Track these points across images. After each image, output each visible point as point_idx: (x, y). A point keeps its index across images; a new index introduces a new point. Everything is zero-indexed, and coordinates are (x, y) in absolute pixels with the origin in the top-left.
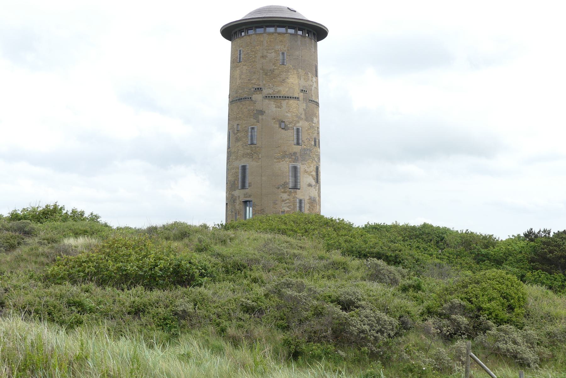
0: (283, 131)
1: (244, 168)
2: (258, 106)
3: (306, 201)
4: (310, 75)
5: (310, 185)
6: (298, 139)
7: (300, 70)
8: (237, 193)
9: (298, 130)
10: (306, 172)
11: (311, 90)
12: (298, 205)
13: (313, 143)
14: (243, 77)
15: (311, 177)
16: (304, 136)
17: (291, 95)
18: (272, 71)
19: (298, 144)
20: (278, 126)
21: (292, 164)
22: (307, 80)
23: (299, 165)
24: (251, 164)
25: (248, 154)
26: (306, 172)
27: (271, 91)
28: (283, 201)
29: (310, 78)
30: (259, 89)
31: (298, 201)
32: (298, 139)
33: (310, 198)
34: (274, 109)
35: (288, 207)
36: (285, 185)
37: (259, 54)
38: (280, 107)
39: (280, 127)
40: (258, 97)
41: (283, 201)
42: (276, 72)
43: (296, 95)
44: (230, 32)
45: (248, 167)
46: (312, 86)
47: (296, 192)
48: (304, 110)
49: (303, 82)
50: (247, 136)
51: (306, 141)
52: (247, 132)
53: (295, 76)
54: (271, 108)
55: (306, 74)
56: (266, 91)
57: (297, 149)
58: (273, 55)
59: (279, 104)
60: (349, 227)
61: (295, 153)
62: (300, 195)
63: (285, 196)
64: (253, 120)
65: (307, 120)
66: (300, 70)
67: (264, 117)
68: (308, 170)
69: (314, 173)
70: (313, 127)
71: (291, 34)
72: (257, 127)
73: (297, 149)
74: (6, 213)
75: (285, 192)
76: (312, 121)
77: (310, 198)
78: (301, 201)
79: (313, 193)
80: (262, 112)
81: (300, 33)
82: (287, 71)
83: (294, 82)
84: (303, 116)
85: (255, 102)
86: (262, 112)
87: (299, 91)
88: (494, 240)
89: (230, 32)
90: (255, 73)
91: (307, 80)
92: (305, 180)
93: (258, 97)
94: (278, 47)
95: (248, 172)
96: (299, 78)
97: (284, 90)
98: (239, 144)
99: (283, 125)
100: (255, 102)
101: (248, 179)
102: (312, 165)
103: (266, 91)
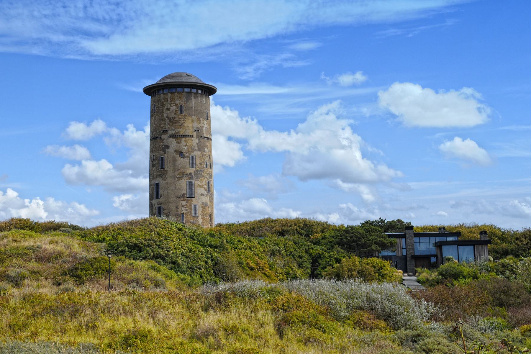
0: (182, 159)
1: (157, 184)
2: (165, 143)
3: (200, 206)
4: (202, 119)
5: (202, 195)
6: (193, 164)
7: (193, 117)
8: (154, 202)
9: (193, 158)
10: (199, 186)
11: (203, 130)
12: (193, 208)
13: (205, 166)
14: (156, 123)
15: (203, 189)
16: (197, 162)
17: (187, 134)
18: (174, 118)
19: (193, 167)
20: (178, 155)
21: (188, 181)
22: (199, 123)
23: (193, 181)
24: (162, 182)
25: (159, 175)
26: (199, 186)
27: (173, 132)
28: (183, 206)
29: (202, 122)
30: (166, 132)
31: (193, 206)
32: (193, 164)
33: (203, 203)
34: (176, 144)
35: (186, 210)
36: (183, 196)
37: (166, 107)
38: (179, 143)
39: (180, 156)
40: (164, 136)
41: (183, 206)
42: (177, 119)
43: (191, 134)
44: (148, 91)
45: (160, 184)
46: (203, 127)
47: (192, 200)
48: (197, 144)
49: (196, 125)
50: (159, 163)
51: (199, 165)
52: (159, 160)
53: (190, 121)
54: (173, 143)
55: (199, 119)
56: (170, 132)
57: (192, 171)
58: (175, 107)
59: (179, 141)
60: (403, 222)
61: (191, 174)
62: (194, 201)
63: (184, 203)
64: (162, 152)
65: (199, 150)
66: (193, 117)
67: (169, 150)
68: (201, 184)
69: (206, 187)
70: (205, 155)
71: (187, 93)
72: (166, 157)
73: (192, 171)
74: (2, 221)
75: (184, 200)
76: (204, 151)
77: (203, 203)
78: (195, 206)
79: (206, 200)
80: (168, 147)
81: (199, 91)
82: (184, 118)
83: (190, 125)
84: (196, 148)
85: (163, 140)
86: (168, 147)
87: (193, 131)
88: (31, 224)
89: (148, 91)
90: (163, 120)
91: (199, 123)
92: (199, 191)
93: (164, 136)
94: (178, 102)
95: (160, 187)
96: (193, 122)
97: (182, 131)
98: (154, 168)
99: (182, 155)
100: (163, 140)
101: (161, 192)
102: (204, 181)
103: (170, 132)
